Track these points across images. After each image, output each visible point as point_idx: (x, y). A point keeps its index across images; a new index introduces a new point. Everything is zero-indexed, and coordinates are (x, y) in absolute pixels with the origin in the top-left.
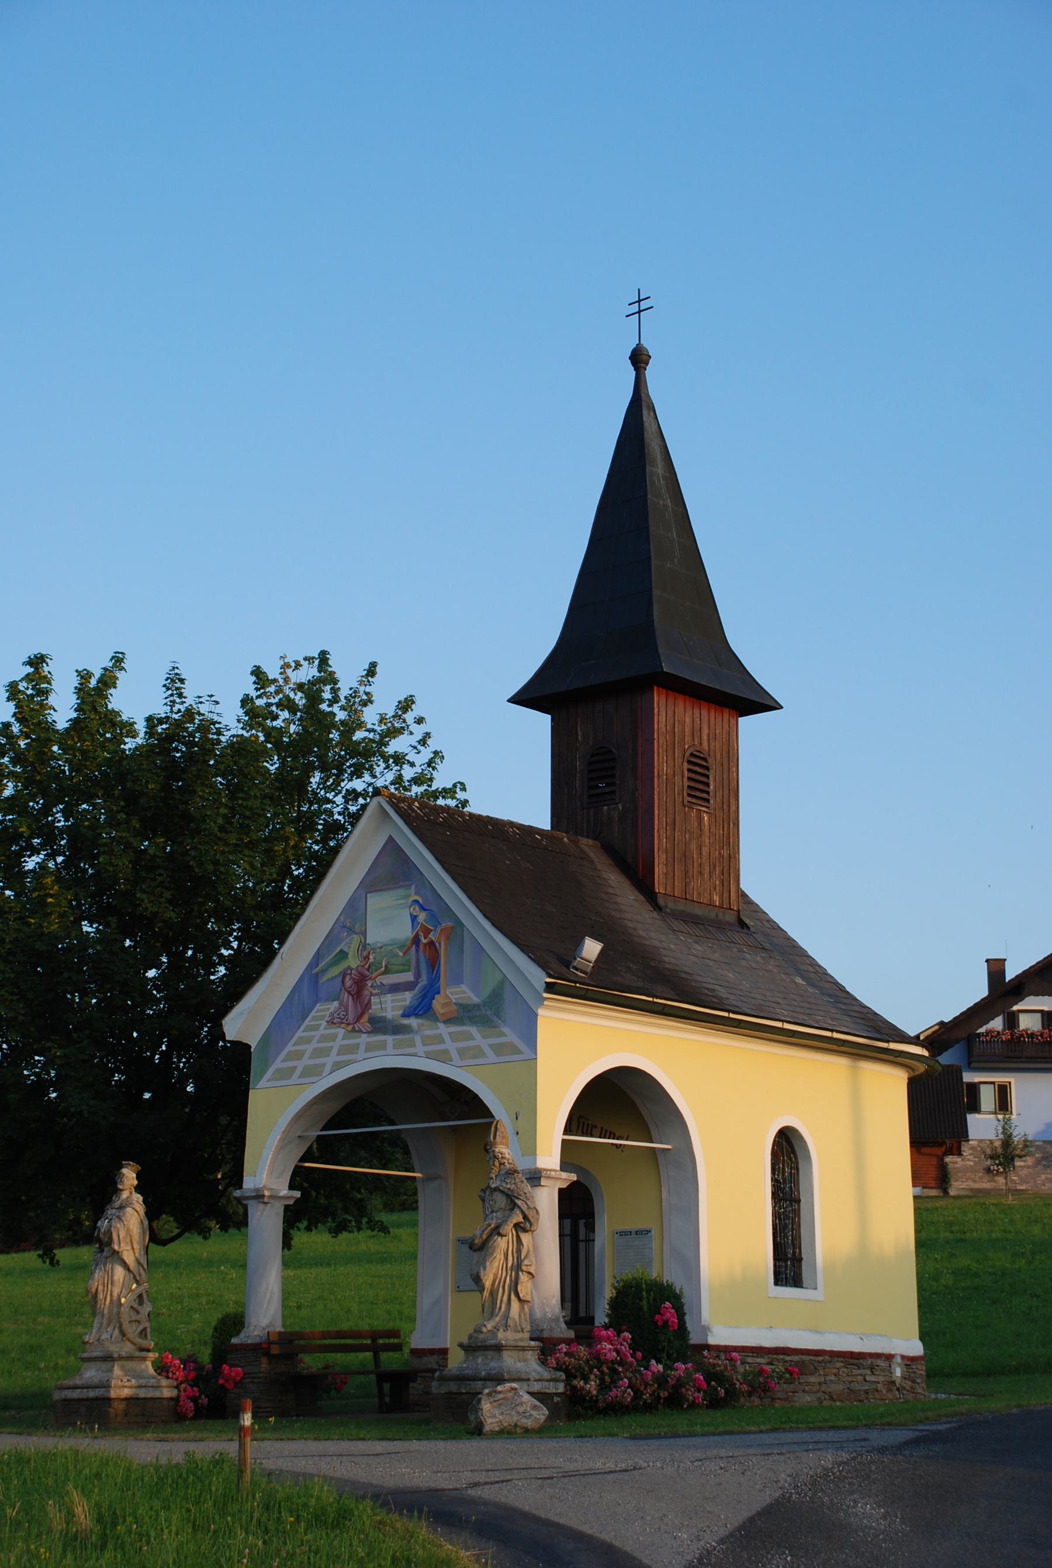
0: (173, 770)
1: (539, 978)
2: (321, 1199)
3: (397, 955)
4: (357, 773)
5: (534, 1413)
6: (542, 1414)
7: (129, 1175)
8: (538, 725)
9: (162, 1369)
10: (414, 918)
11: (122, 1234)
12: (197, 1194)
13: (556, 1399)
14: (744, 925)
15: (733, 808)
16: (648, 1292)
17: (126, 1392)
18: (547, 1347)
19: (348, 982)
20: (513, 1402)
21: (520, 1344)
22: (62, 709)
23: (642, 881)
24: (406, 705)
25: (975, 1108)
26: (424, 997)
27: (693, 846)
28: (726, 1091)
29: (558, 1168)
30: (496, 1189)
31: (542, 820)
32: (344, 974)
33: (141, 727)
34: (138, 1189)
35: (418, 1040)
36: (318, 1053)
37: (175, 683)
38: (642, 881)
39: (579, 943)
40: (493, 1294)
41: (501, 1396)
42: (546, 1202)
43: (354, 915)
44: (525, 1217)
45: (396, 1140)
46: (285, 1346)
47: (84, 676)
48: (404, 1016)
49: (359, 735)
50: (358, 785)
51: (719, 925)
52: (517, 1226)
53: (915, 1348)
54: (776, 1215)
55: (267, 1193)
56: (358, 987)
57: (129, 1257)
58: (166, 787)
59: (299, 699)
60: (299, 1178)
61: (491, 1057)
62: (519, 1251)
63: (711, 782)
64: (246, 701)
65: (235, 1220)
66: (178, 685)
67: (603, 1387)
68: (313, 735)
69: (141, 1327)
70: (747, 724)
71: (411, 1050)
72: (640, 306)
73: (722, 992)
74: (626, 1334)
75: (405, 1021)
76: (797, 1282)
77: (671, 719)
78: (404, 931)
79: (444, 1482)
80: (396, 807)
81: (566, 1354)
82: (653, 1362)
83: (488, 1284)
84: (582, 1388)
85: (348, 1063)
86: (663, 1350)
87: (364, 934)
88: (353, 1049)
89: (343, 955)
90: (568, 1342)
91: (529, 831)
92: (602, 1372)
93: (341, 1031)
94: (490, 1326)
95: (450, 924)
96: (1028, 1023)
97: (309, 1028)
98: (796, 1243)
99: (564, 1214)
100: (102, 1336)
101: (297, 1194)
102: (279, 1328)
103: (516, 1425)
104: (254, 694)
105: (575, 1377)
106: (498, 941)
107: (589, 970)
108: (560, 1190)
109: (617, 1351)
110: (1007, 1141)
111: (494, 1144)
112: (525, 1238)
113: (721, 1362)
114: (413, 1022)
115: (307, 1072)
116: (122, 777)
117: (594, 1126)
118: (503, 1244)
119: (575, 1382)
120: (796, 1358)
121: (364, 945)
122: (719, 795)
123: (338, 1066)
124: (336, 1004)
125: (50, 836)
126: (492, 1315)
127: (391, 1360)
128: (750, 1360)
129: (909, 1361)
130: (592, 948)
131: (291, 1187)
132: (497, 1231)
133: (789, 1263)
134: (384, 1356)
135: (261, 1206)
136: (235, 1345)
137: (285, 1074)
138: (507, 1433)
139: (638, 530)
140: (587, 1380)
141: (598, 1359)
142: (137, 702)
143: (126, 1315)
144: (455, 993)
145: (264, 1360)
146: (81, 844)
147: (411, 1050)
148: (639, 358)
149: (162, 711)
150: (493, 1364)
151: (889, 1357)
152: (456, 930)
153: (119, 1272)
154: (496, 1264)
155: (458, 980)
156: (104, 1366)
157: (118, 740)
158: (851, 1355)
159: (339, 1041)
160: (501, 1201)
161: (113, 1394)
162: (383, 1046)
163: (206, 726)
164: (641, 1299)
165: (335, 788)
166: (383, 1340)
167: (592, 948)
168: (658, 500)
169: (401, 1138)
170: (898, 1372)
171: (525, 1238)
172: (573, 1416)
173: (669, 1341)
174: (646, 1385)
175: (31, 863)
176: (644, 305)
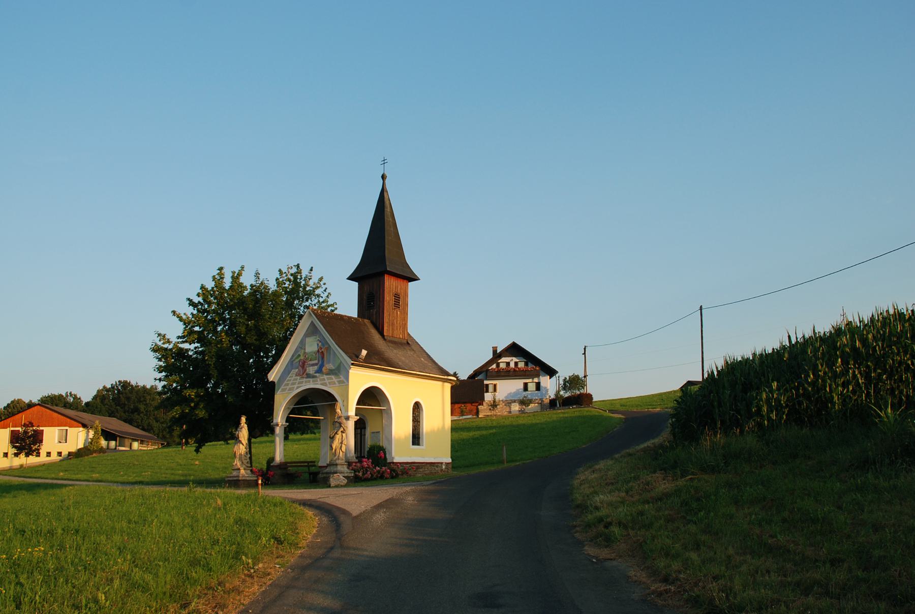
0: (257, 301)
2: (294, 426)
4: (307, 301)
6: (345, 481)
7: (243, 419)
8: (355, 285)
12: (261, 426)
14: (408, 343)
18: (349, 464)
20: (338, 479)
22: (227, 283)
23: (381, 333)
24: (321, 279)
25: (487, 391)
28: (401, 391)
31: (355, 315)
33: (249, 287)
36: (293, 384)
37: (257, 275)
38: (381, 333)
42: (350, 426)
43: (302, 344)
45: (315, 408)
46: (283, 466)
47: (234, 272)
49: (308, 288)
50: (307, 304)
51: (402, 344)
53: (450, 460)
56: (303, 365)
58: (254, 306)
59: (292, 278)
60: (288, 419)
61: (337, 384)
63: (400, 301)
64: (277, 279)
65: (272, 431)
67: (363, 474)
68: (296, 289)
72: (384, 162)
76: (418, 444)
77: (391, 284)
78: (315, 348)
79: (313, 498)
89: (299, 355)
91: (350, 318)
96: (503, 366)
98: (419, 434)
100: (237, 463)
110: (494, 401)
113: (395, 467)
115: (290, 389)
116: (243, 303)
118: (338, 437)
123: (298, 388)
125: (224, 320)
127: (313, 469)
129: (447, 464)
130: (364, 352)
132: (336, 433)
133: (416, 438)
137: (284, 390)
141: (363, 467)
142: (247, 280)
143: (243, 458)
144: (329, 366)
146: (233, 324)
148: (384, 177)
149: (254, 283)
152: (329, 348)
155: (329, 362)
157: (242, 292)
160: (337, 425)
163: (266, 287)
165: (300, 305)
167: (364, 352)
168: (388, 218)
169: (314, 408)
172: (355, 482)
175: (219, 328)
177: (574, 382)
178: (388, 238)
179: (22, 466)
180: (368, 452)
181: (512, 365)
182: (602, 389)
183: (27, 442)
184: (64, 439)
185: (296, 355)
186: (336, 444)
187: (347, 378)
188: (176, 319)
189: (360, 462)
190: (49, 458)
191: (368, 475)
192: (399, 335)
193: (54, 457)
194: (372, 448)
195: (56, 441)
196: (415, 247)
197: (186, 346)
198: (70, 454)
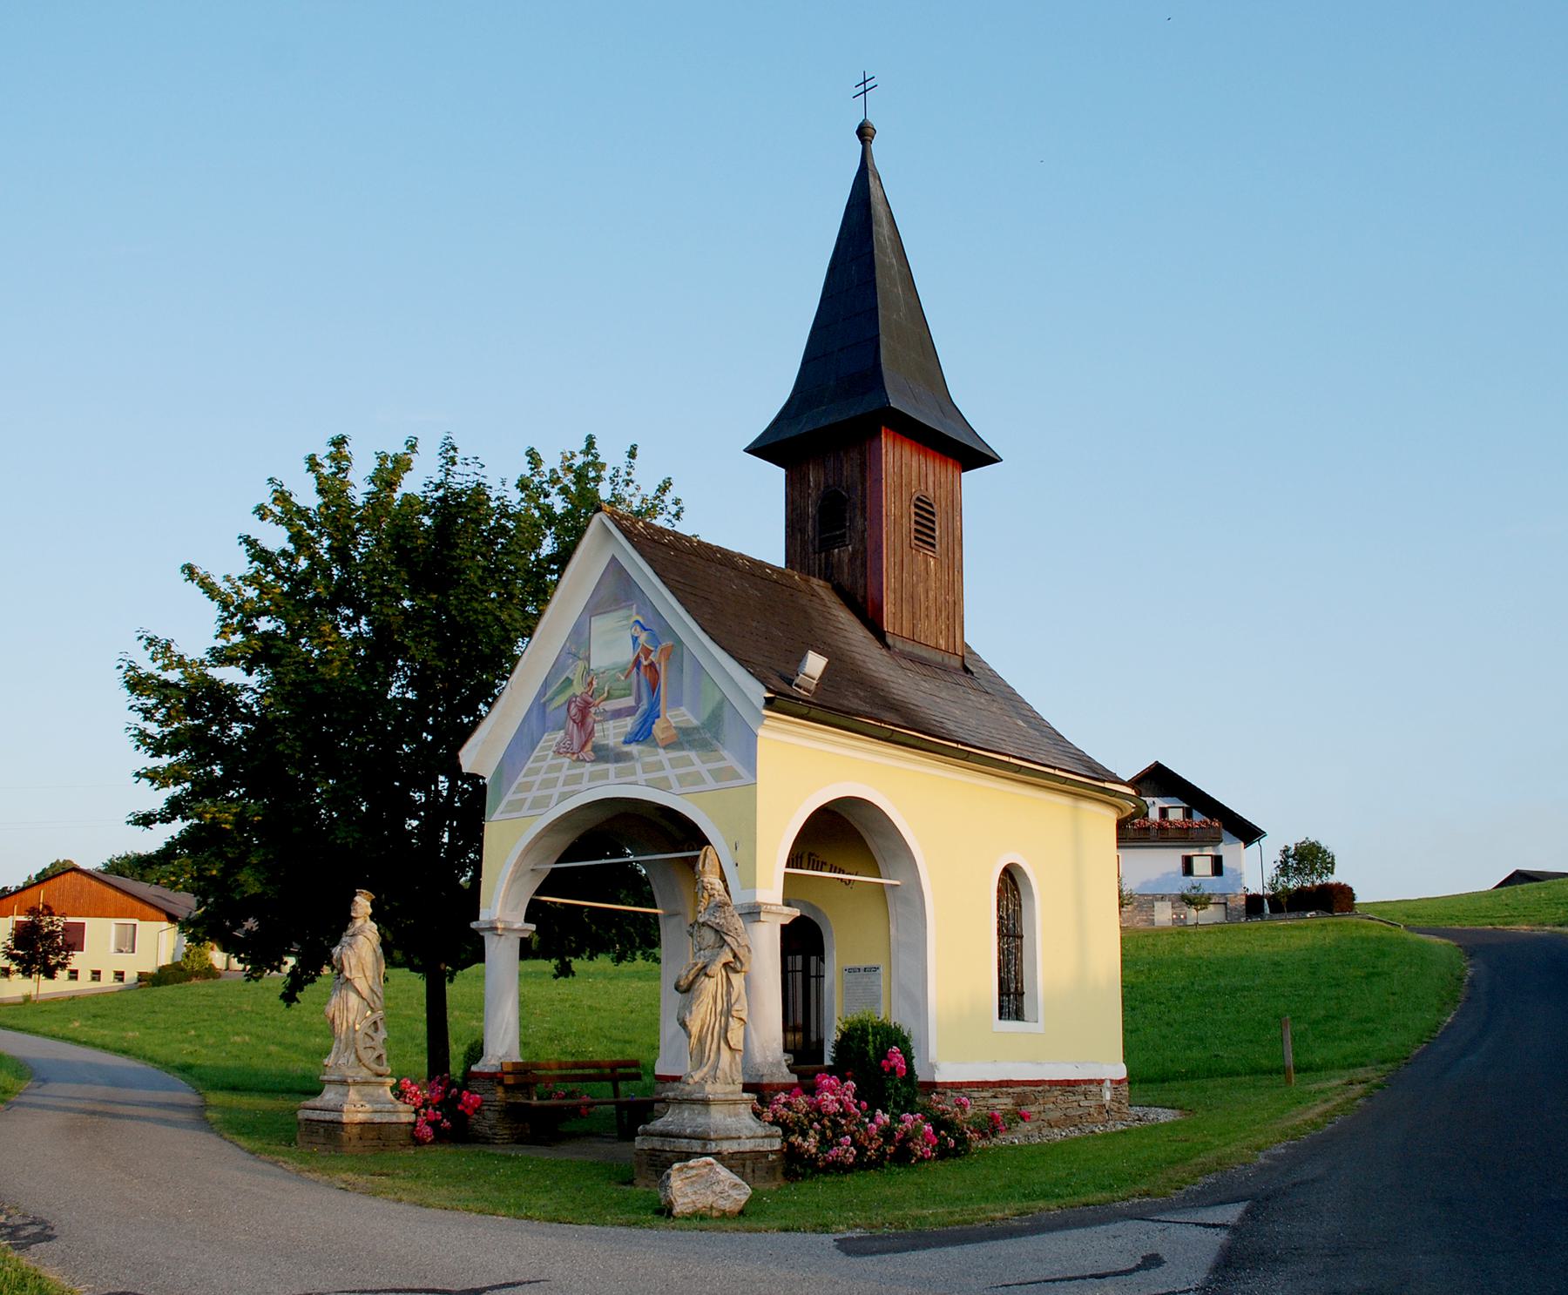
1: (758, 693)
2: (557, 935)
3: (618, 680)
5: (734, 1193)
7: (363, 904)
8: (774, 477)
9: (399, 1093)
10: (635, 639)
11: (353, 962)
12: (436, 936)
13: (771, 1157)
15: (957, 556)
16: (874, 1035)
17: (360, 1117)
18: (759, 1091)
19: (574, 711)
21: (730, 1097)
23: (872, 621)
24: (664, 488)
26: (645, 721)
27: (921, 589)
29: (780, 902)
30: (704, 924)
31: (779, 560)
32: (569, 703)
34: (372, 917)
35: (638, 766)
36: (547, 784)
38: (872, 621)
39: (801, 658)
40: (701, 1041)
41: (694, 1172)
43: (579, 639)
44: (735, 956)
46: (522, 1076)
48: (625, 742)
51: (945, 669)
52: (726, 965)
53: (1120, 1072)
54: (1001, 951)
55: (499, 925)
56: (582, 715)
57: (361, 984)
60: (534, 912)
61: (711, 783)
62: (729, 994)
63: (934, 526)
66: (452, 453)
67: (825, 1143)
69: (376, 1054)
70: (973, 481)
71: (632, 779)
72: (865, 86)
73: (951, 726)
74: (850, 1083)
75: (627, 748)
76: (1018, 1015)
77: (898, 463)
78: (626, 655)
80: (618, 525)
81: (784, 1105)
82: (879, 1112)
83: (695, 1030)
84: (800, 1146)
85: (573, 793)
86: (889, 1098)
87: (588, 659)
88: (577, 779)
90: (787, 1088)
91: (761, 565)
92: (823, 1126)
93: (566, 761)
94: (697, 1076)
95: (670, 643)
97: (537, 760)
98: (1019, 979)
99: (787, 950)
101: (533, 927)
102: (516, 1057)
103: (712, 1207)
104: (528, 473)
105: (794, 1133)
106: (737, 679)
107: (813, 688)
108: (783, 927)
109: (840, 1102)
111: (703, 873)
112: (737, 980)
114: (634, 749)
117: (824, 863)
118: (710, 987)
119: (792, 1139)
120: (1018, 1090)
121: (588, 671)
122: (944, 541)
123: (564, 797)
124: (562, 733)
126: (700, 1064)
128: (976, 1095)
130: (815, 664)
131: (528, 919)
132: (703, 971)
134: (622, 1086)
135: (496, 938)
136: (475, 1073)
137: (517, 805)
138: (700, 1217)
139: (863, 287)
140: (804, 1135)
141: (818, 1110)
144: (675, 716)
145: (500, 1090)
147: (632, 779)
148: (864, 133)
150: (700, 1120)
151: (1100, 1082)
152: (676, 650)
153: (353, 997)
154: (703, 1010)
155: (677, 702)
156: (341, 1089)
158: (1069, 1083)
159: (565, 772)
160: (709, 937)
161: (345, 1119)
162: (604, 775)
164: (867, 1043)
166: (624, 1071)
167: (815, 664)
170: (1108, 1096)
171: (737, 980)
173: (897, 1088)
174: (871, 1140)
176: (868, 85)
177: (1309, 856)
178: (889, 317)
179: (27, 998)
180: (840, 1047)
181: (1154, 815)
182: (1375, 874)
183: (38, 948)
184: (128, 944)
185: (556, 679)
186: (702, 1013)
187: (750, 761)
188: (194, 589)
189: (808, 1086)
190: (95, 984)
191: (845, 1150)
192: (931, 632)
193: (107, 981)
194: (854, 1037)
195: (112, 948)
196: (978, 341)
197: (231, 675)
198: (142, 977)
